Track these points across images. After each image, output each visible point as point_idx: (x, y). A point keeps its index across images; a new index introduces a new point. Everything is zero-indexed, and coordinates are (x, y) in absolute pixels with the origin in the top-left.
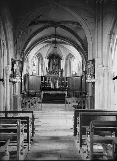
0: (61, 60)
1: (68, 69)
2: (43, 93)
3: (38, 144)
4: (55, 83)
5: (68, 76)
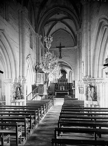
0: (66, 74)
1: (71, 79)
2: (56, 93)
3: (6, 95)
4: (62, 88)
5: (70, 83)
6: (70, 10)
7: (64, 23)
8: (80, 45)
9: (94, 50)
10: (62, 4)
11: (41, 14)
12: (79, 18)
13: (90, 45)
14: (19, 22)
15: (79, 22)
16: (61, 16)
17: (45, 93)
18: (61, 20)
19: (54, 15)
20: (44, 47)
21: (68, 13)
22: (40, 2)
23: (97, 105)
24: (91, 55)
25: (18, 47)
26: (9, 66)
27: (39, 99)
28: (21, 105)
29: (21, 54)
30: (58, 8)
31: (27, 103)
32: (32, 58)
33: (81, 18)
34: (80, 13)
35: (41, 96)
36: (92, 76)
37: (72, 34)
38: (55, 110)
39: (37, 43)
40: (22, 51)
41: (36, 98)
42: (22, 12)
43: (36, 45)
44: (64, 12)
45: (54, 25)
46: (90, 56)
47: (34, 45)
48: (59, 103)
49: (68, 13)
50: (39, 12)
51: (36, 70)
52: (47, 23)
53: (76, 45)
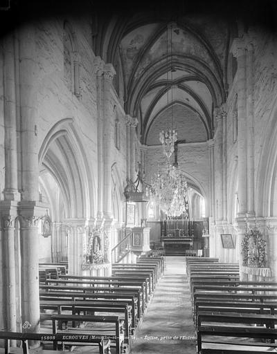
6: (201, 63)
7: (184, 88)
8: (224, 140)
9: (263, 157)
10: (184, 50)
11: (137, 73)
12: (222, 82)
13: (253, 146)
14: (98, 97)
15: (222, 90)
16: (179, 74)
17: (146, 248)
18: (179, 83)
19: (164, 74)
20: (140, 143)
21: (196, 69)
22: (135, 48)
23: (268, 277)
24: (256, 167)
25: (97, 151)
26: (78, 192)
27: (132, 259)
28: (101, 275)
29: (102, 164)
30: (175, 59)
31: (192, 274)
32: (119, 169)
33: (226, 81)
34: (224, 69)
35: (138, 253)
36: (257, 213)
37: (202, 111)
38: (168, 288)
39: (129, 136)
40: (104, 156)
41: (125, 258)
42: (103, 74)
43: (125, 142)
44: (188, 67)
45: (163, 94)
46: (253, 170)
47: (122, 142)
48: (176, 268)
49: (196, 69)
50: (133, 69)
51: (127, 197)
52: (150, 89)
53: (212, 138)
